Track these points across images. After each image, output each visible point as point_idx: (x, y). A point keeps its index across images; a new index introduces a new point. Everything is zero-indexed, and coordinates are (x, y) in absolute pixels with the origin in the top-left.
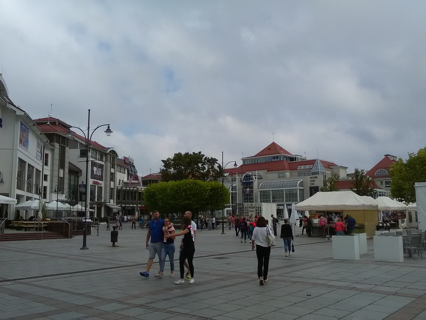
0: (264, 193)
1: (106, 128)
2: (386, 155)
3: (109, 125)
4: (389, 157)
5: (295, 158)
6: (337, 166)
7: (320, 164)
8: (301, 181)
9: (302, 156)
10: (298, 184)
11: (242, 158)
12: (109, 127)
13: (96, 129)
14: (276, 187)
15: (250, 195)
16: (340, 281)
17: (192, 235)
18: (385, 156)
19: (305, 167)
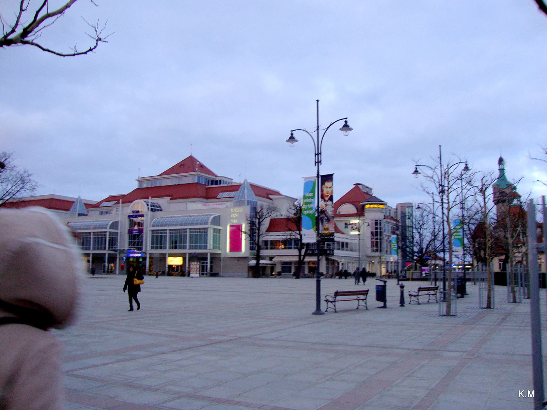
0: (131, 234)
1: (342, 123)
2: (357, 185)
3: (346, 118)
4: (360, 186)
5: (220, 181)
6: (282, 195)
7: (248, 190)
8: (217, 215)
9: (232, 179)
10: (210, 221)
11: (137, 178)
12: (346, 122)
13: (328, 128)
14: (197, 224)
15: (138, 235)
16: (251, 304)
17: (384, 268)
18: (354, 185)
19: (229, 195)
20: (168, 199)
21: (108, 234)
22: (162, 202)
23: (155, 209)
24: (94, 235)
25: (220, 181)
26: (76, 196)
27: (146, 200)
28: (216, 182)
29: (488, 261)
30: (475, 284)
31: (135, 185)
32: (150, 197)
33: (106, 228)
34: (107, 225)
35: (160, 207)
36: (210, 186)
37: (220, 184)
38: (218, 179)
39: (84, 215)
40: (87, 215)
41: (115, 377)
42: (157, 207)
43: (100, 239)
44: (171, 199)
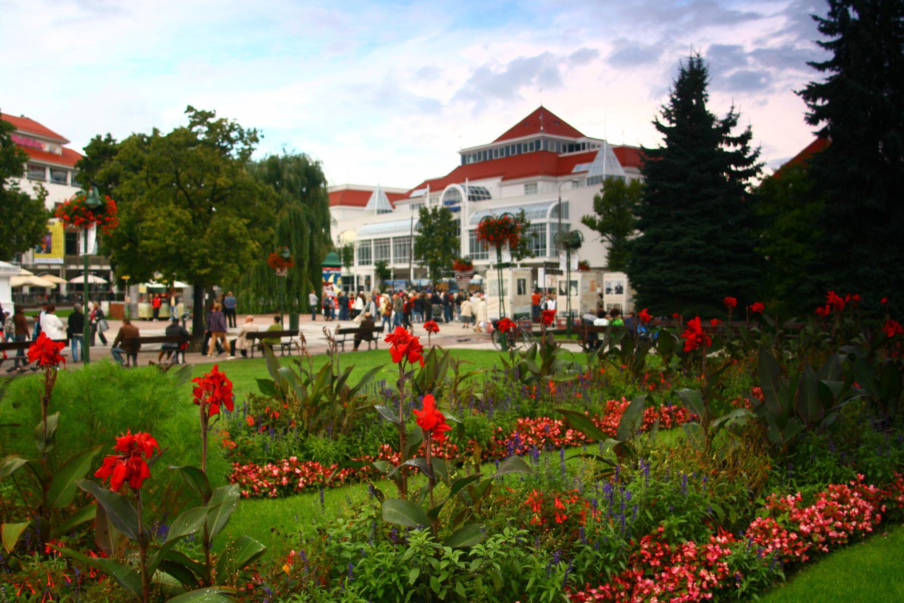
7: (608, 157)
20: (498, 180)
21: (548, 227)
22: (490, 184)
23: (477, 196)
24: (395, 242)
25: (584, 144)
26: (375, 185)
27: (463, 184)
28: (578, 147)
29: (656, 276)
30: (314, 319)
31: (457, 162)
32: (467, 180)
33: (544, 216)
34: (545, 212)
35: (488, 193)
36: (567, 154)
37: (584, 148)
38: (580, 141)
39: (386, 212)
40: (391, 211)
41: (265, 475)
42: (482, 193)
43: (383, 249)
44: (503, 180)
